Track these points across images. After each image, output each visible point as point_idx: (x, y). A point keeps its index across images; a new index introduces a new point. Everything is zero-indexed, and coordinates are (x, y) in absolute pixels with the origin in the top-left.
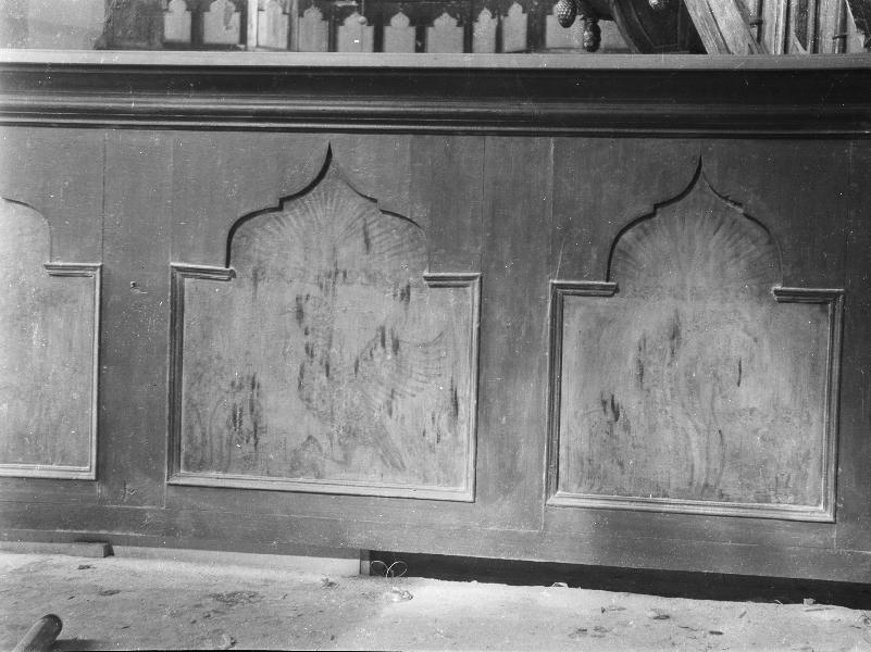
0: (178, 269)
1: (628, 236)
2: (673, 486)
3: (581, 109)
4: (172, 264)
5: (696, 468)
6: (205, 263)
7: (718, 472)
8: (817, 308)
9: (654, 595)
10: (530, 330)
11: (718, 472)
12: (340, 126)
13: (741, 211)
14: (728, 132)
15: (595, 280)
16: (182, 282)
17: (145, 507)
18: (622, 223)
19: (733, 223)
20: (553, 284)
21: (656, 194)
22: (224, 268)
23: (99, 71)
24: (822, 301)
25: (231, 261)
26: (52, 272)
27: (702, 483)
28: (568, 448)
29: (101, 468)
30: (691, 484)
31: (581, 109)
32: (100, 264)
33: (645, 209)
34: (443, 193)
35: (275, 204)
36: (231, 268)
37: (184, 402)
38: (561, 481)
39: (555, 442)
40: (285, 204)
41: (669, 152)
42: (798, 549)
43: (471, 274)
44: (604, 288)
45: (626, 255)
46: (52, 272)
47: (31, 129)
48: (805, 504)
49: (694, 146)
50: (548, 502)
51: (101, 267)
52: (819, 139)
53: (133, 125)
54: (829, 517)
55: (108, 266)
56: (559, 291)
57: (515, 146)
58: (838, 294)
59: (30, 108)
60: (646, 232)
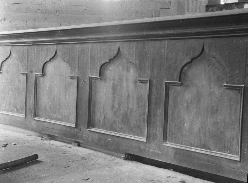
0: (91, 77)
1: (186, 68)
2: (196, 144)
3: (172, 32)
4: (89, 76)
5: (202, 140)
6: (96, 76)
7: (208, 141)
8: (237, 91)
9: (159, 167)
10: (160, 94)
11: (208, 141)
12: (175, 38)
13: (215, 60)
14: (232, 35)
15: (176, 81)
16: (92, 80)
17: (84, 135)
18: (183, 64)
19: (213, 64)
20: (166, 82)
21: (191, 56)
22: (99, 77)
23: (15, 35)
24: (239, 89)
25: (101, 75)
26: (71, 78)
27: (203, 143)
28: (169, 130)
29: (76, 125)
30: (200, 144)
31: (172, 32)
32: (77, 76)
33: (189, 60)
34: (142, 56)
35: (49, 60)
36: (101, 77)
37: (92, 110)
38: (168, 139)
39: (166, 128)
40: (193, 60)
41: (195, 44)
42: (229, 168)
43: (147, 79)
44: (178, 83)
45: (185, 74)
46: (71, 78)
47: (174, 40)
48: (232, 154)
49: (201, 41)
50: (163, 145)
51: (244, 87)
52: (201, 38)
53: (190, 38)
54: (238, 159)
55: (79, 77)
56: (168, 84)
57: (158, 43)
58: (242, 87)
59: (115, 37)
60: (190, 68)
